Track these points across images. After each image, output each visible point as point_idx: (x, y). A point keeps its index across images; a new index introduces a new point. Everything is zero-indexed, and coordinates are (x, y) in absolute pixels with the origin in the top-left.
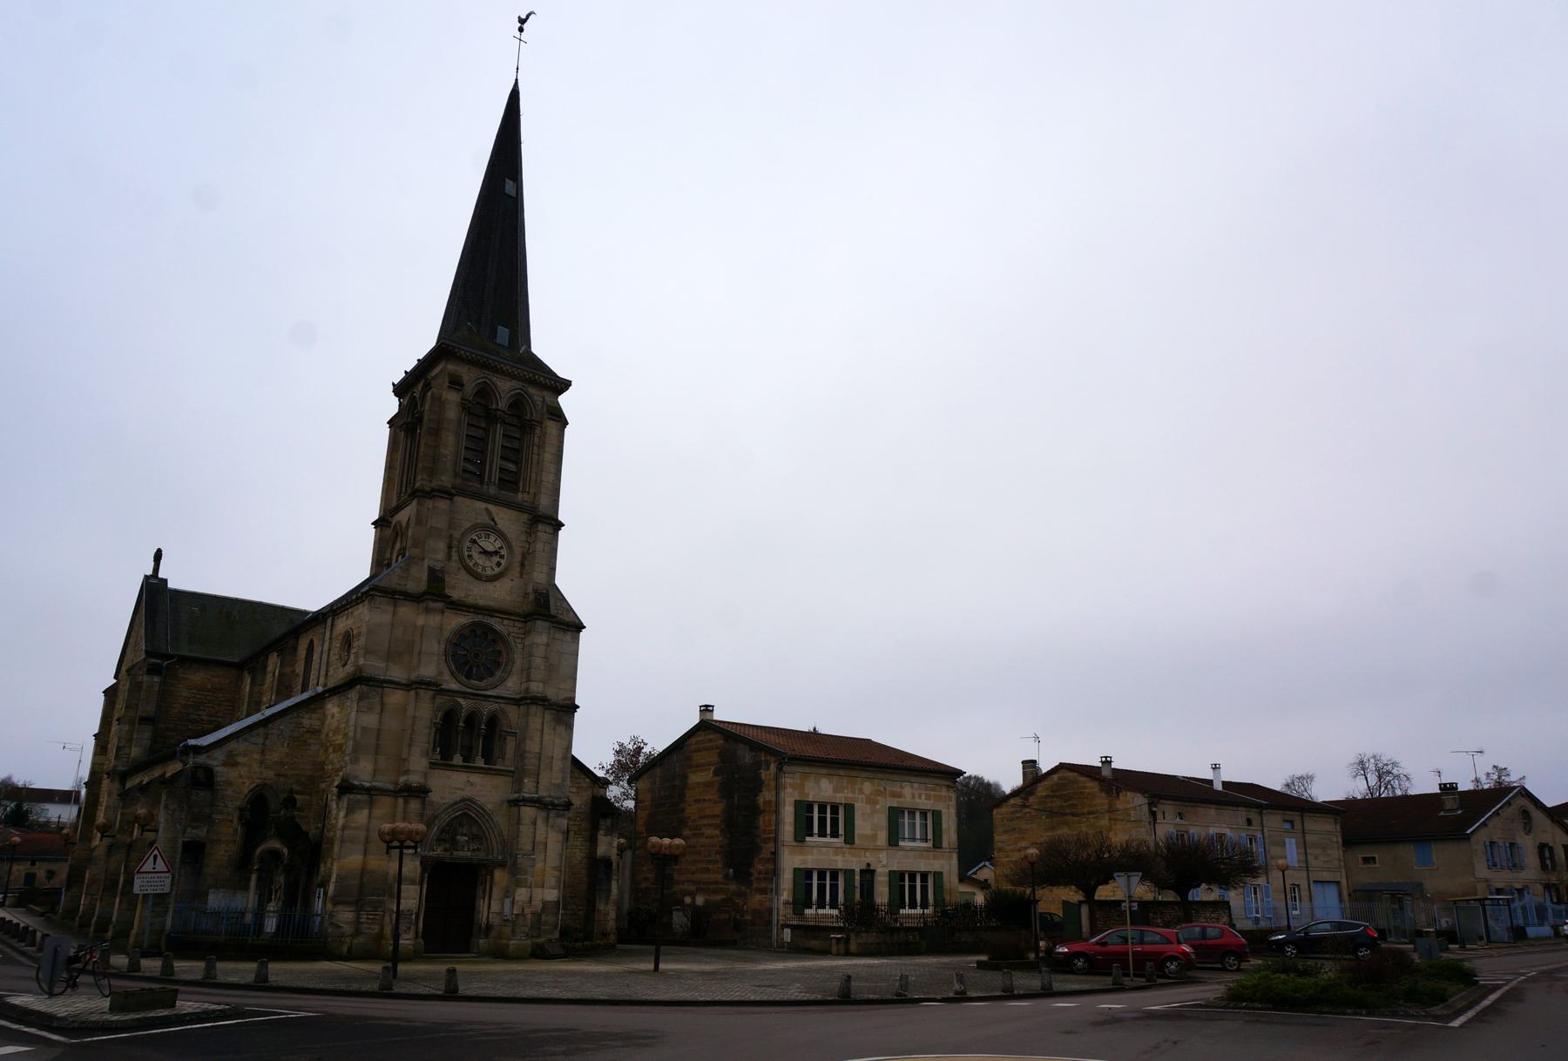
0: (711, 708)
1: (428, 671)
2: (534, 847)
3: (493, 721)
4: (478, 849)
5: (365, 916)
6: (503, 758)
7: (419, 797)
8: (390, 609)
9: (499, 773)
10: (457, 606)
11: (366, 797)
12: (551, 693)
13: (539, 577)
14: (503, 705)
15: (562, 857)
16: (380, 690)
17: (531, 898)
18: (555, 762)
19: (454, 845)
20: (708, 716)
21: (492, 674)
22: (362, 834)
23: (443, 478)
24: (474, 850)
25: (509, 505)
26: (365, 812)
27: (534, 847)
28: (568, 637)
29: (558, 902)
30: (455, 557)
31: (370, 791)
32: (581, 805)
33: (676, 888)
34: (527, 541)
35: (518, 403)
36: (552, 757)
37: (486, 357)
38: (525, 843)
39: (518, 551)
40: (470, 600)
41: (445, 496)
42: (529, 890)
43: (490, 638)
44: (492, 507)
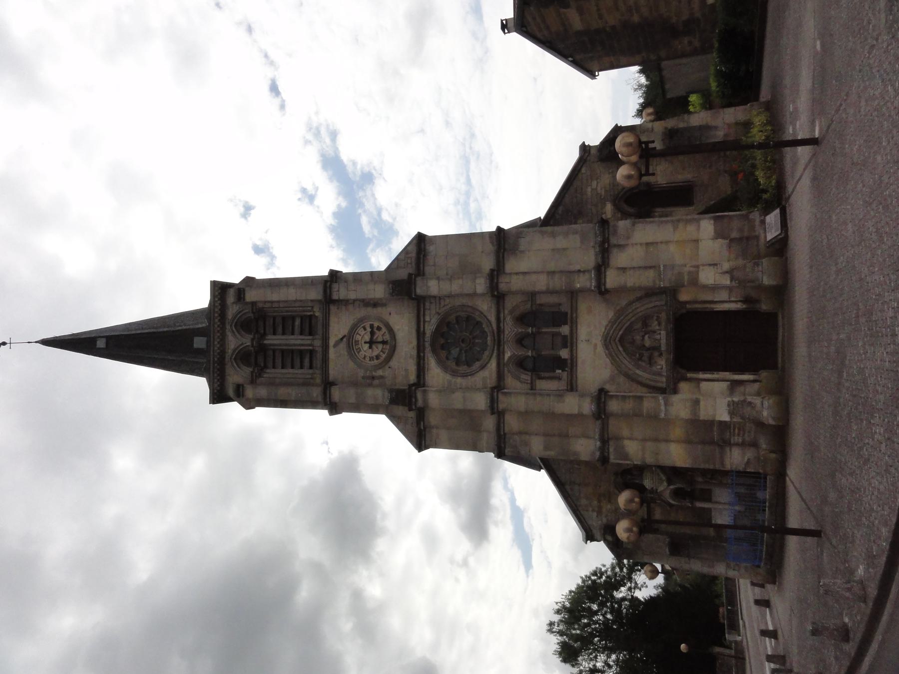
0: (504, 22)
1: (480, 401)
2: (651, 267)
3: (522, 319)
4: (658, 319)
5: (736, 438)
6: (560, 304)
7: (604, 402)
8: (434, 431)
9: (574, 308)
10: (421, 370)
11: (611, 443)
12: (488, 264)
13: (379, 292)
14: (506, 312)
15: (662, 222)
16: (507, 436)
17: (710, 265)
18: (559, 246)
19: (656, 348)
20: (511, 25)
21: (479, 324)
22: (649, 444)
23: (315, 395)
24: (659, 324)
25: (326, 326)
26: (627, 443)
27: (651, 267)
28: (431, 248)
29: (716, 219)
30: (380, 373)
31: (605, 441)
32: (609, 173)
33: (698, 15)
34: (354, 303)
35: (244, 325)
36: (553, 250)
37: (214, 364)
38: (646, 279)
39: (362, 312)
40: (414, 353)
41: (328, 392)
42: (701, 268)
43: (445, 329)
44: (332, 342)
